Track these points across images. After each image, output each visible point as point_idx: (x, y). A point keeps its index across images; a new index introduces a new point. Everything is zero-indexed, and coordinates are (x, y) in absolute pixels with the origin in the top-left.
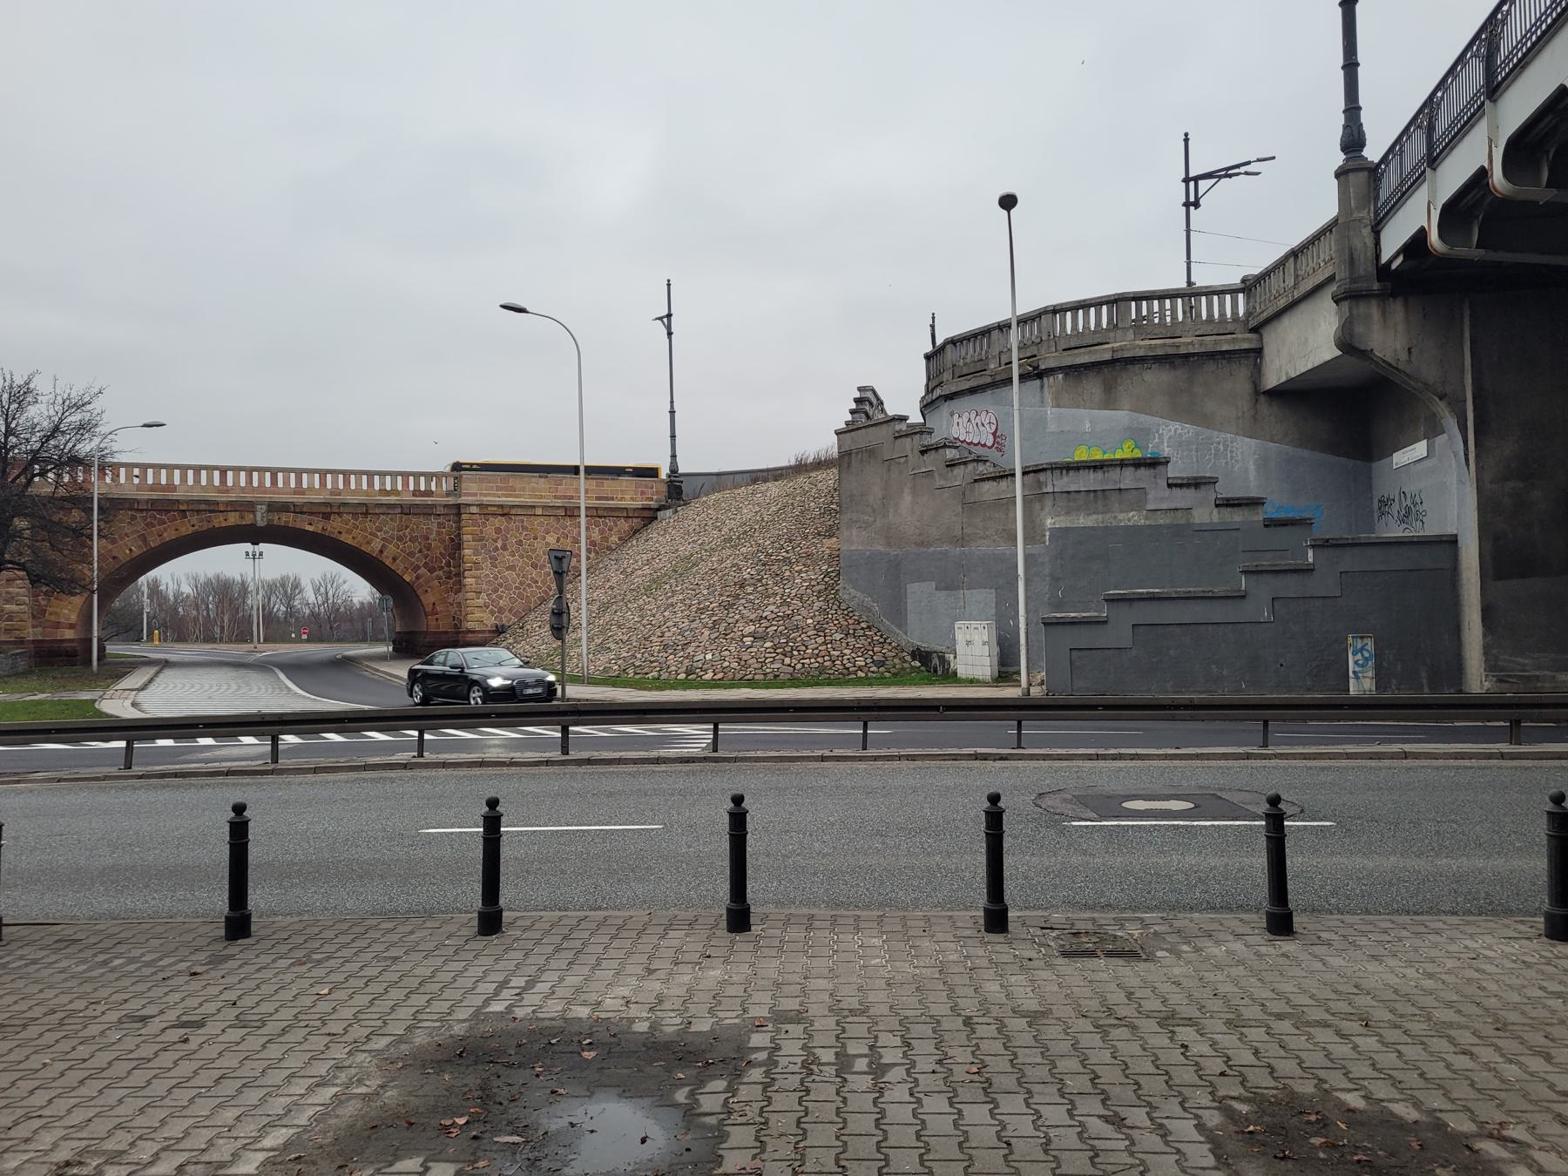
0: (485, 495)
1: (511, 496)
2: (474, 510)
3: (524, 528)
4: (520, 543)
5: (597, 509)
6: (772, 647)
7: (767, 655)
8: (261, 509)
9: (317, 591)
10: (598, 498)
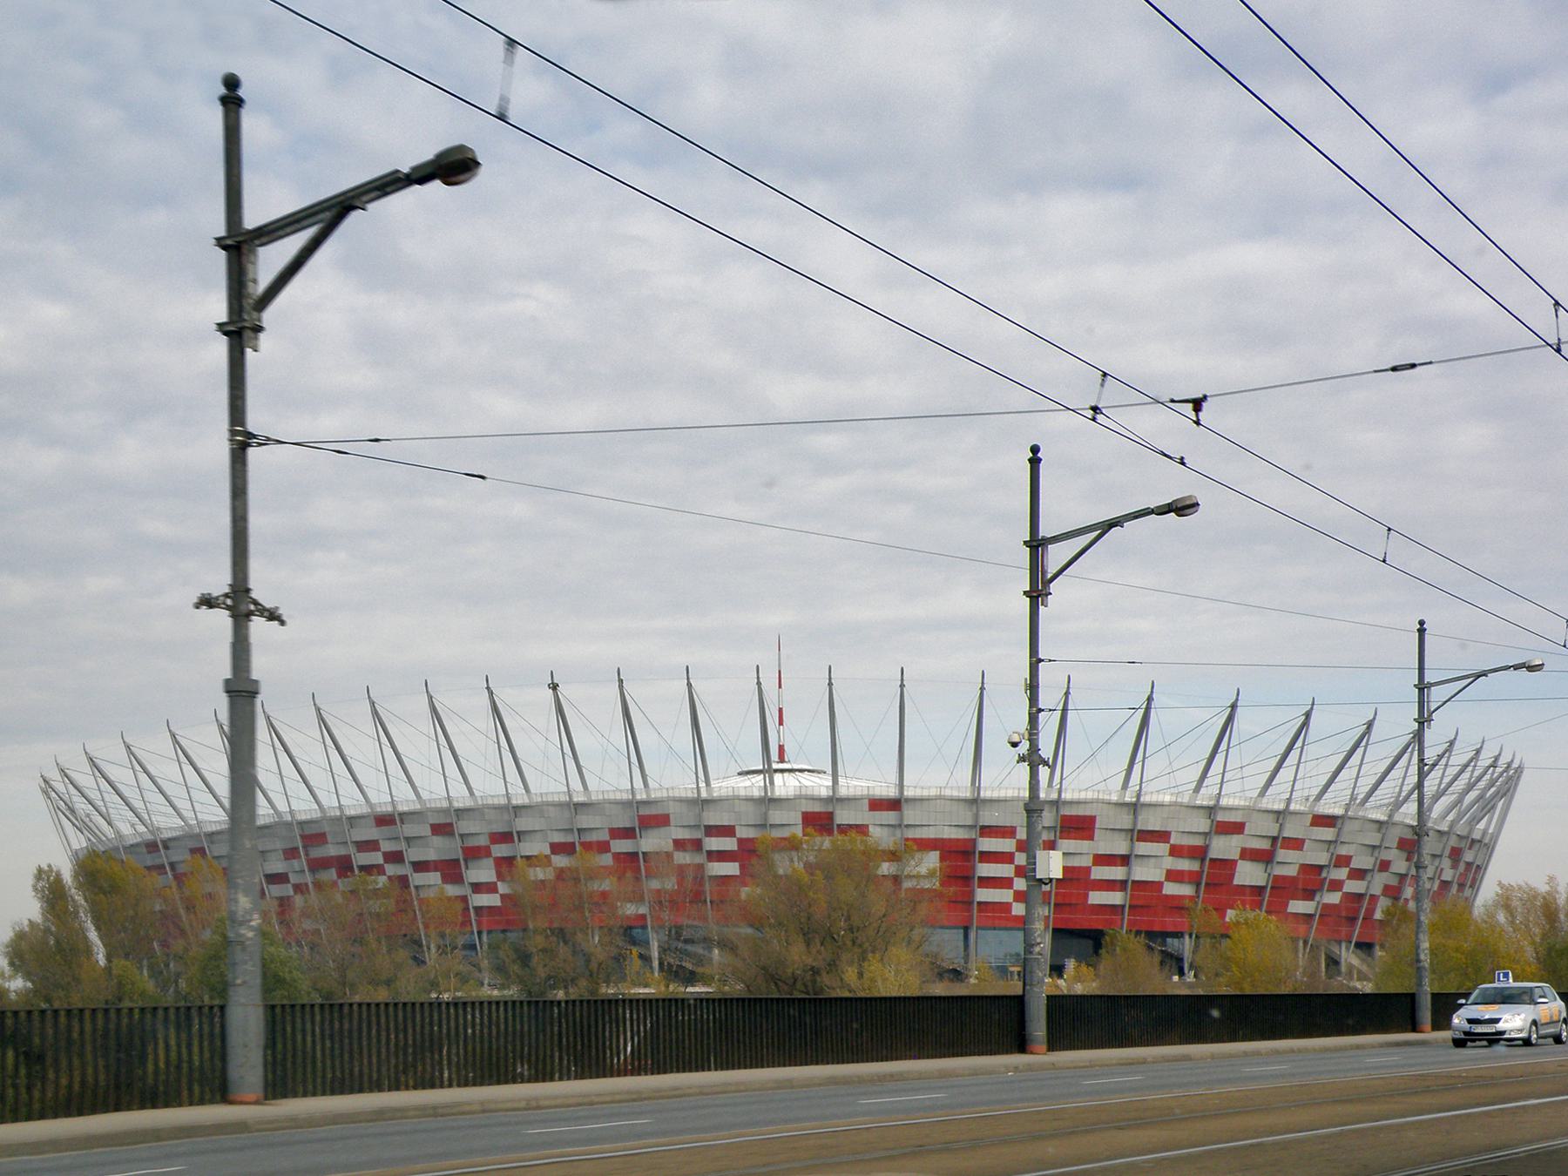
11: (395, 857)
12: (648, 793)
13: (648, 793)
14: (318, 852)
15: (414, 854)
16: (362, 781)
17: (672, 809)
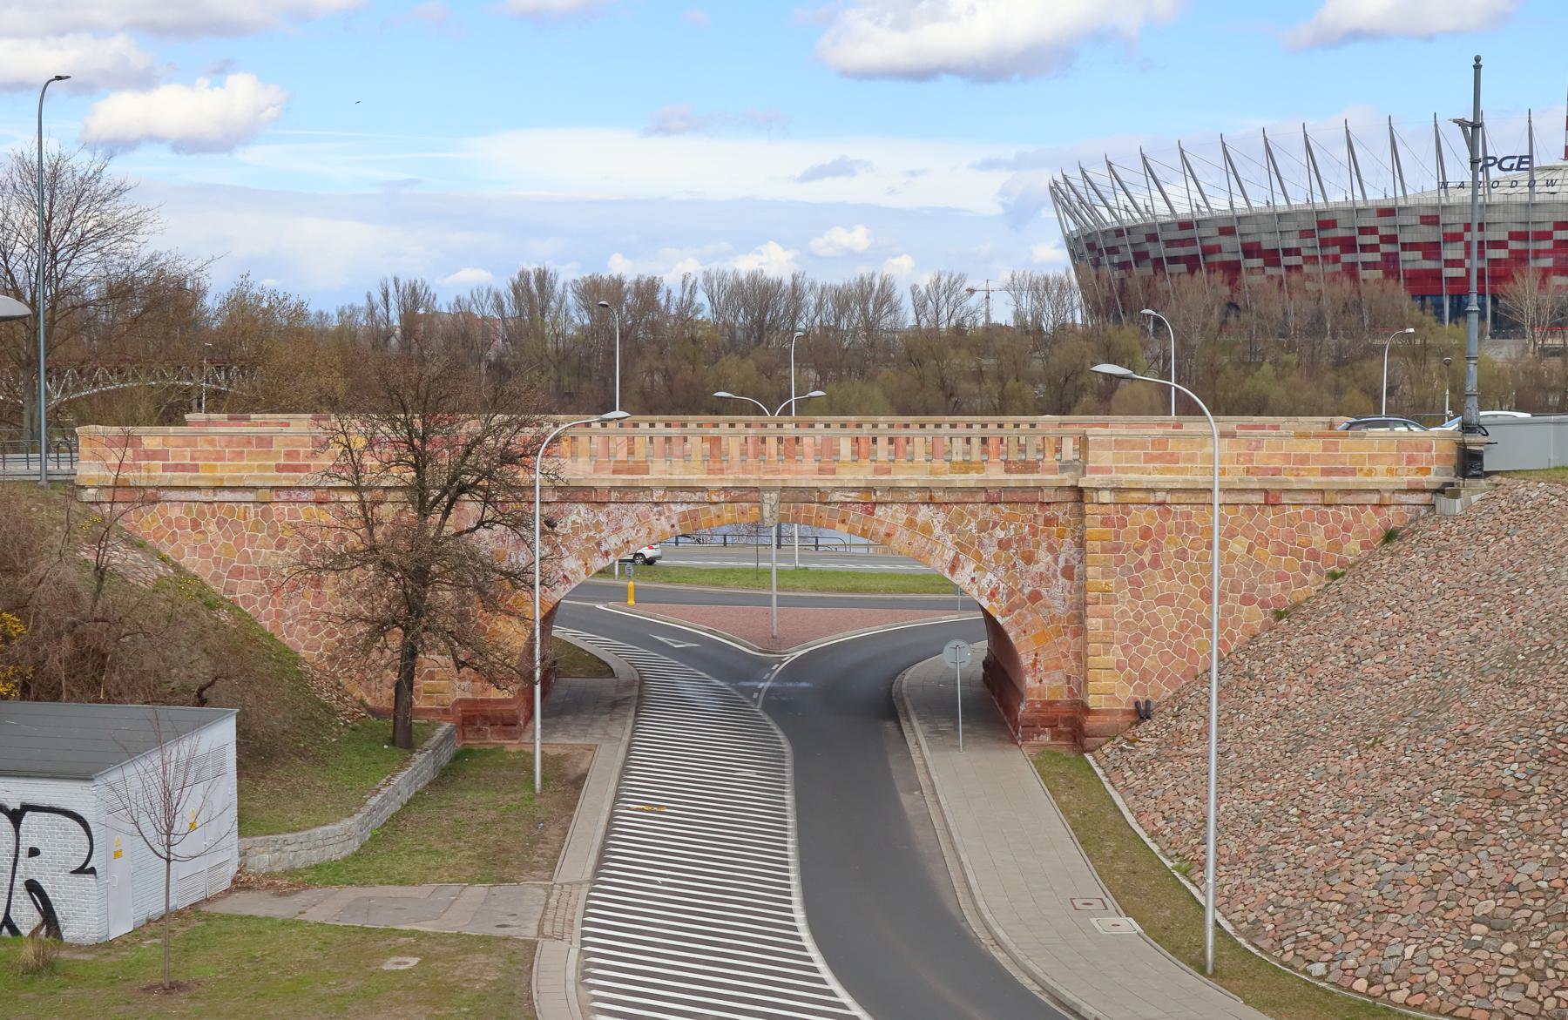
0: (1125, 471)
1: (1169, 471)
2: (1105, 497)
3: (1191, 529)
4: (1182, 555)
5: (1322, 491)
6: (1512, 955)
7: (1503, 971)
8: (771, 498)
9: (920, 307)
10: (1326, 472)
11: (1392, 239)
12: (1406, 202)
13: (1406, 202)
14: (1329, 234)
15: (1406, 237)
16: (1405, 181)
17: (1339, 216)
